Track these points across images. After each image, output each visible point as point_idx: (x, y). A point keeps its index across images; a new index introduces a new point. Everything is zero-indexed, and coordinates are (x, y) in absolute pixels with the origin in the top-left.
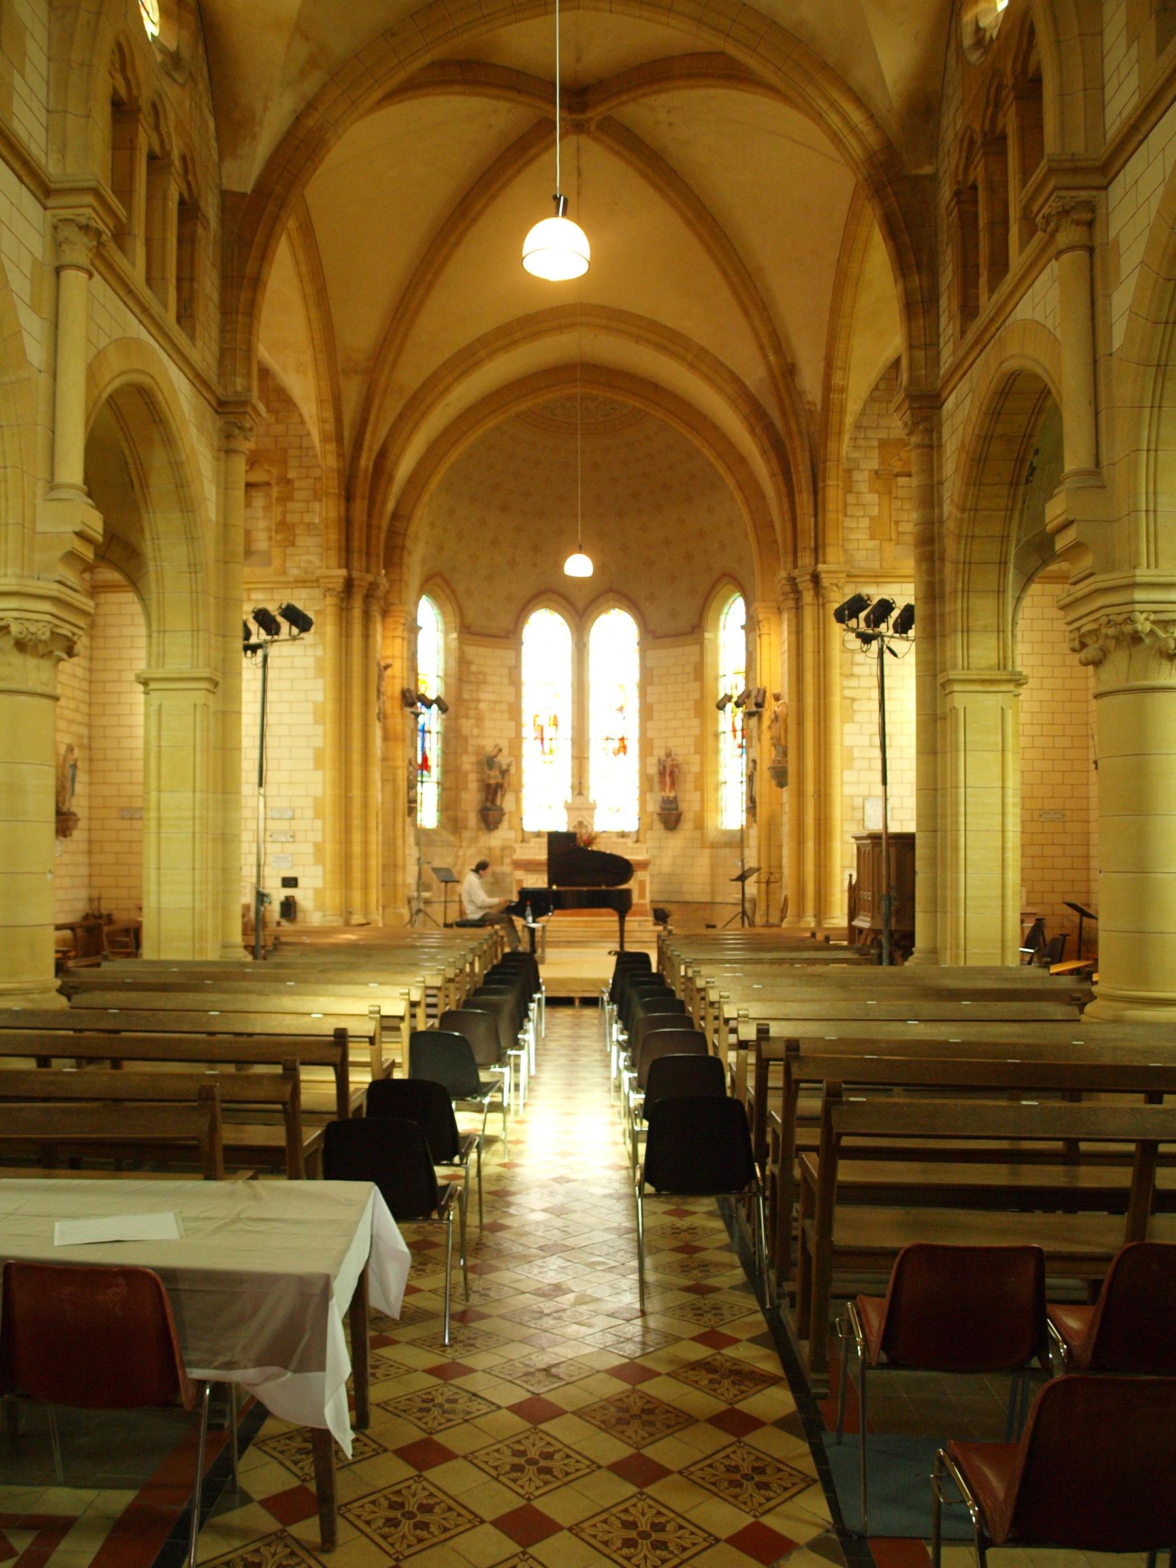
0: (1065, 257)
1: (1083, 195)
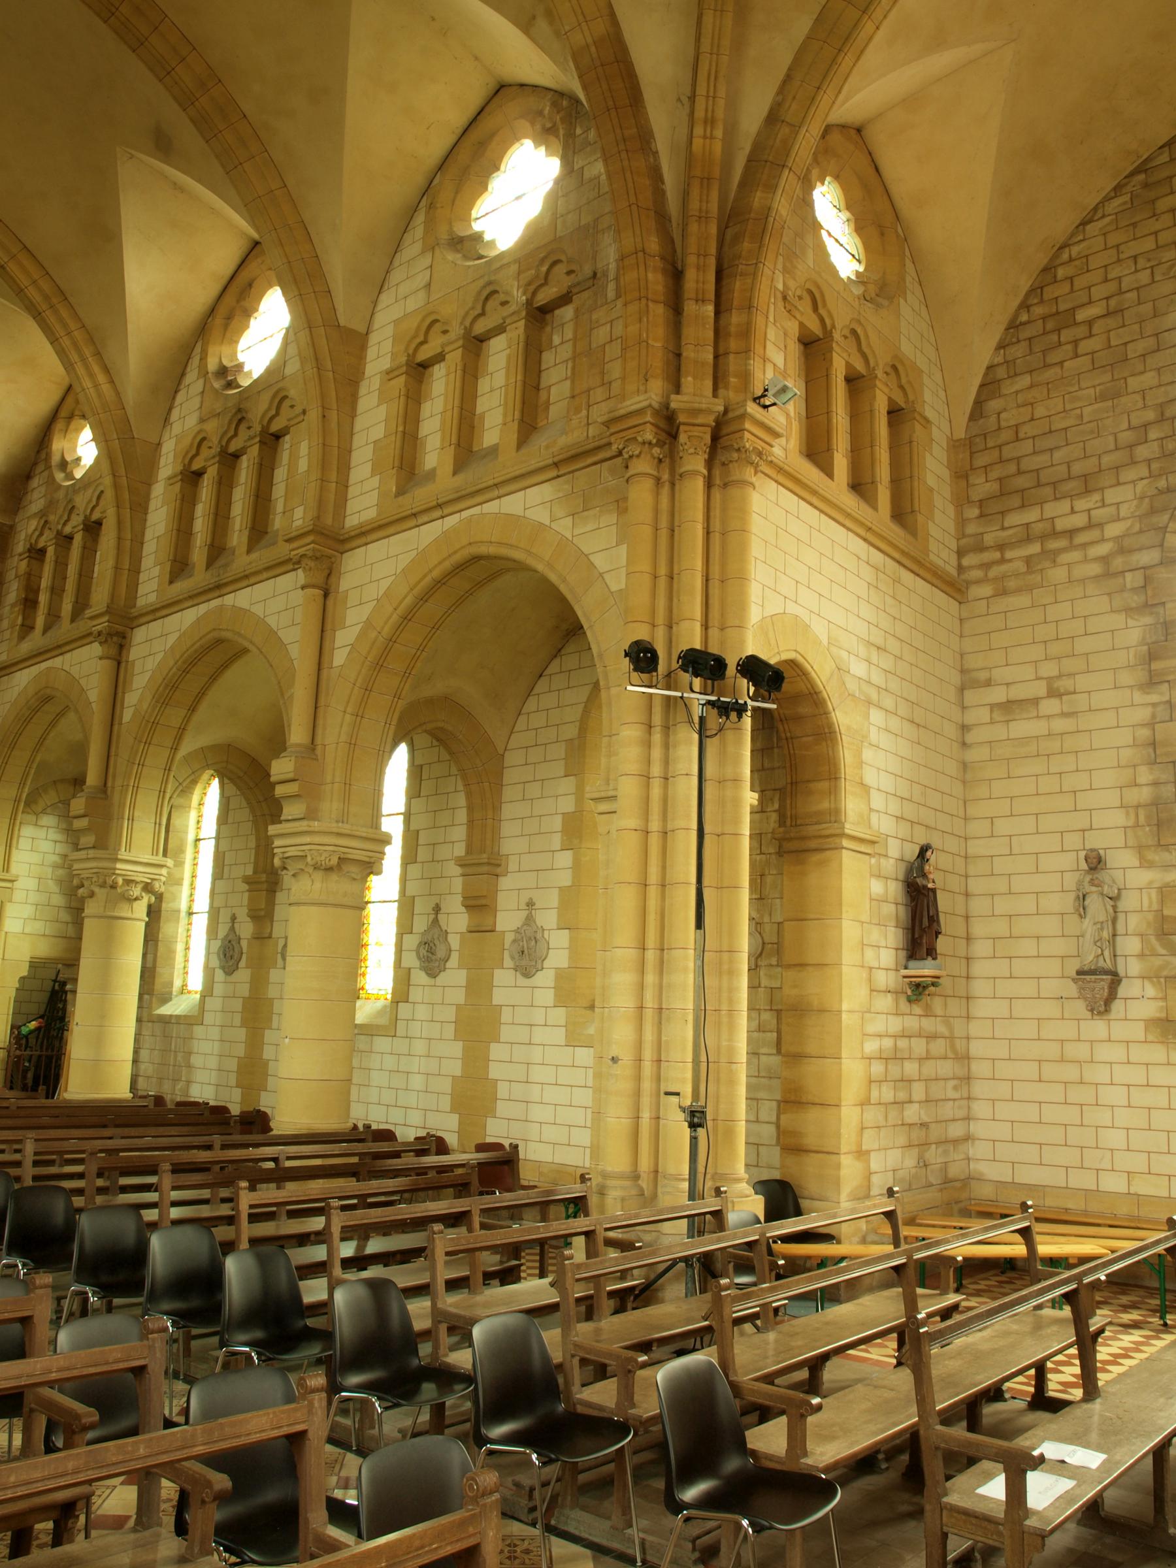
0: (309, 591)
1: (120, 628)
